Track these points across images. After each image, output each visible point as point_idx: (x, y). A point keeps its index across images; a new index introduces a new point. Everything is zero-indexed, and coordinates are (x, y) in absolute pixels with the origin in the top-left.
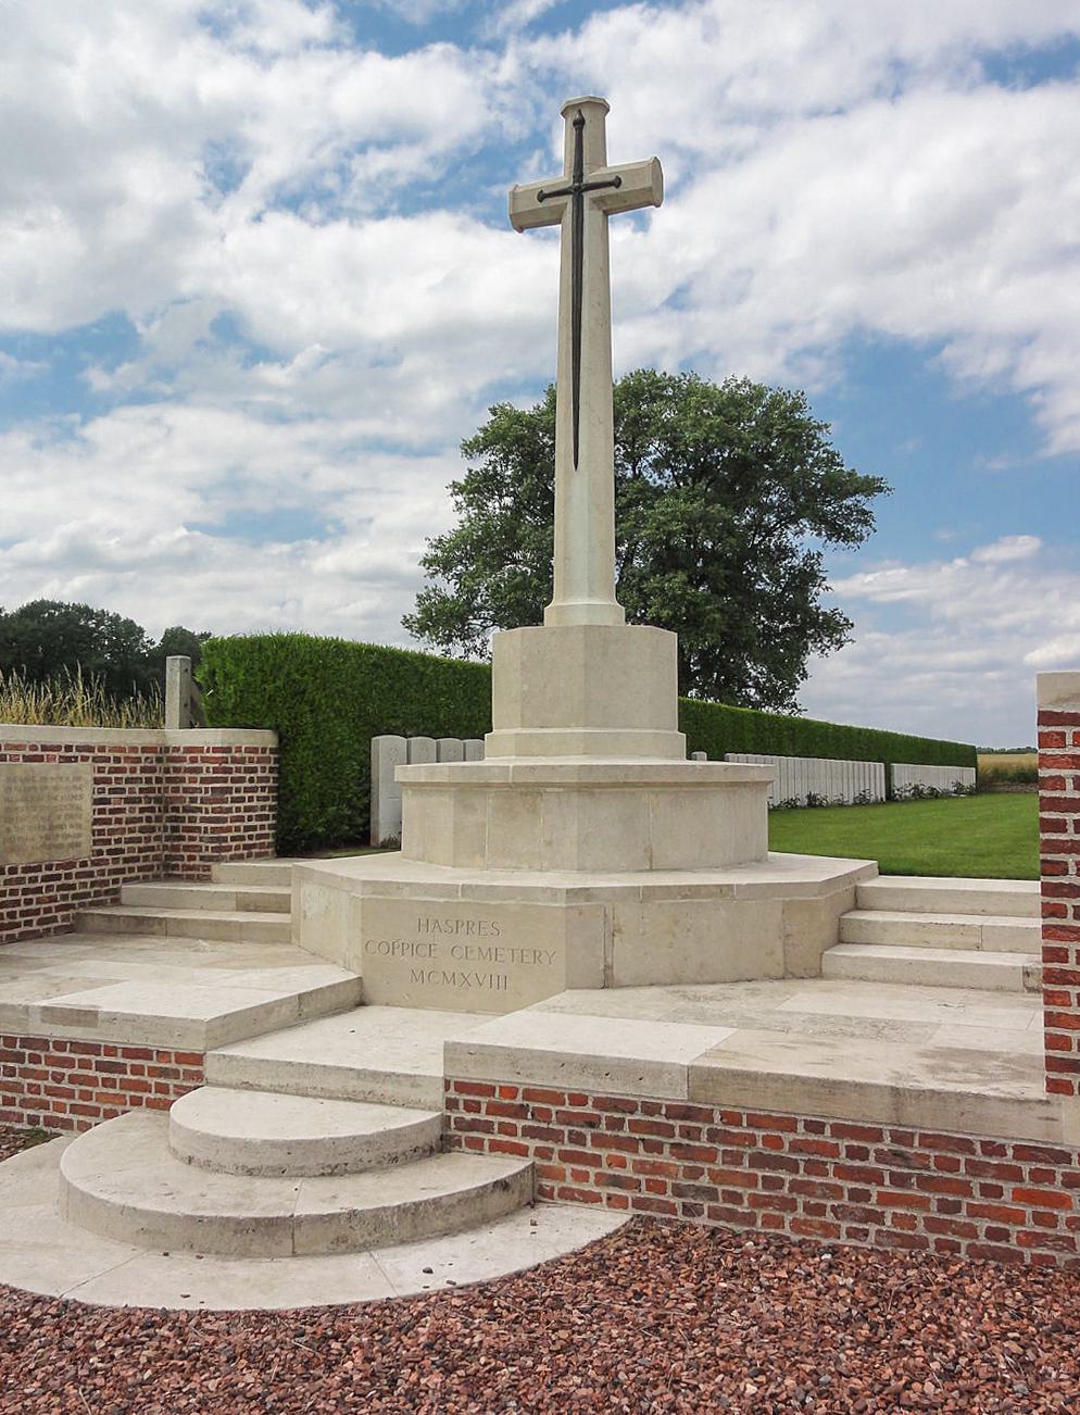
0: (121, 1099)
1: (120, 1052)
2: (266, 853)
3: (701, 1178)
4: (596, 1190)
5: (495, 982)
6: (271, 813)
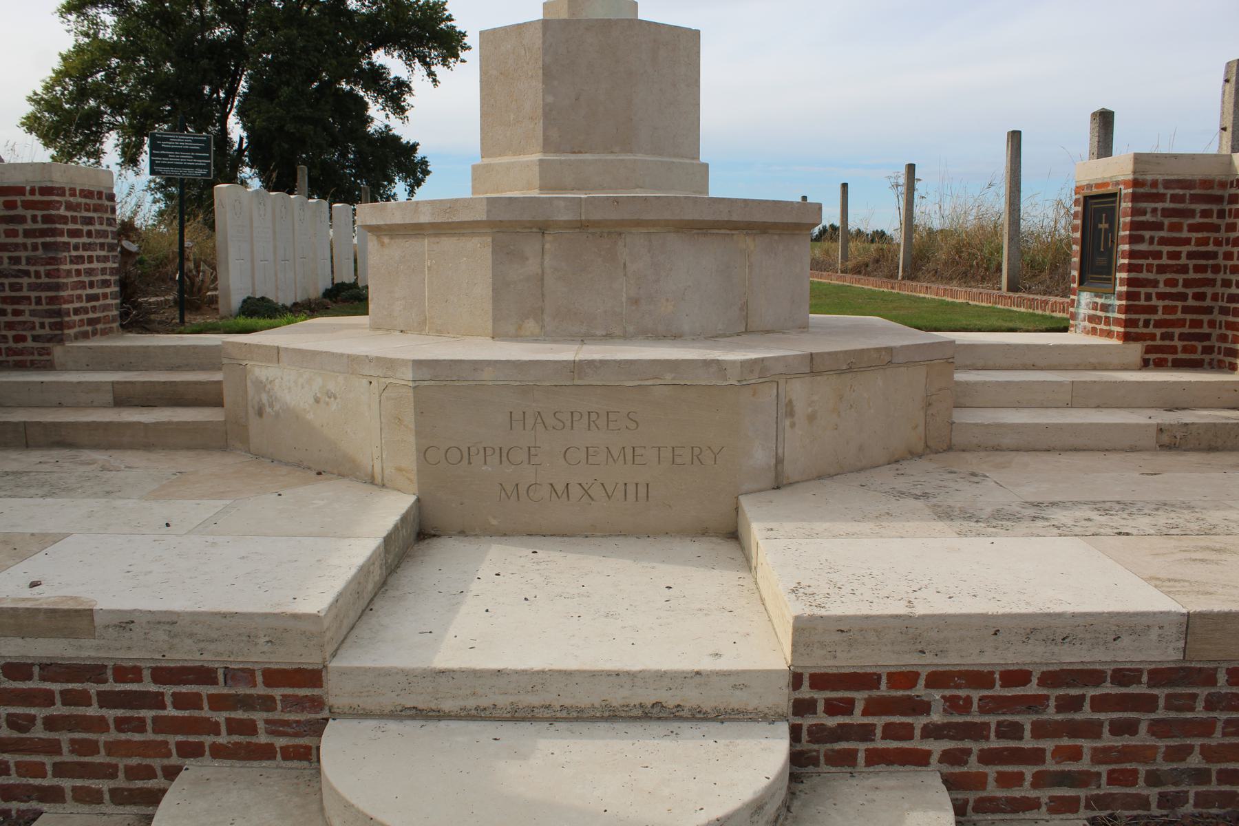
0: (161, 749)
1: (146, 674)
2: (111, 330)
3: (1189, 759)
4: (1033, 794)
5: (642, 491)
6: (113, 278)
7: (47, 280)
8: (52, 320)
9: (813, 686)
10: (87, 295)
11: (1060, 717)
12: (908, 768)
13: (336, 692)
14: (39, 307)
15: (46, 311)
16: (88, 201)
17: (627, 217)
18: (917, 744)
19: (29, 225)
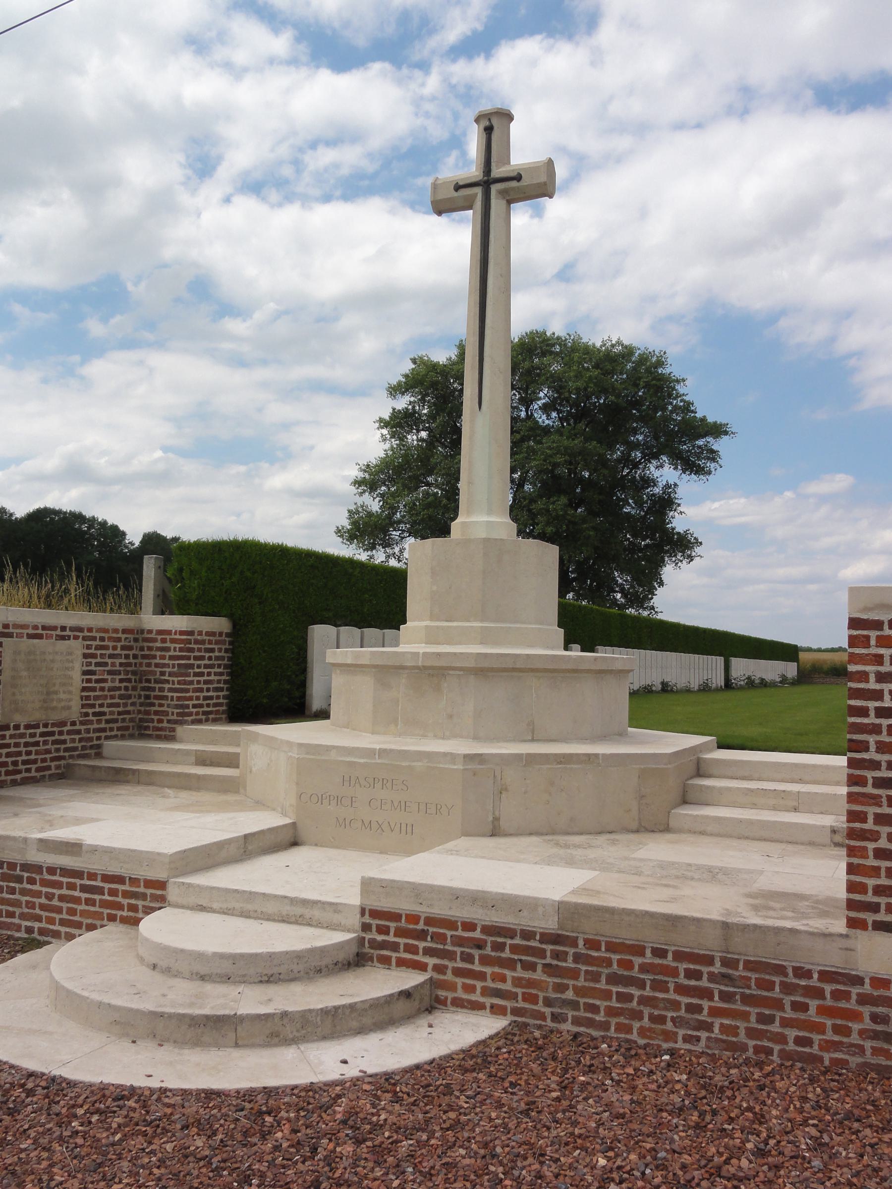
3: (567, 993)
5: (409, 829)
6: (225, 686)
7: (178, 686)
8: (178, 711)
9: (370, 916)
10: (204, 697)
11: (493, 954)
12: (416, 971)
13: (172, 893)
14: (172, 703)
15: (176, 705)
16: (211, 638)
17: (444, 665)
18: (420, 958)
19: (172, 653)
